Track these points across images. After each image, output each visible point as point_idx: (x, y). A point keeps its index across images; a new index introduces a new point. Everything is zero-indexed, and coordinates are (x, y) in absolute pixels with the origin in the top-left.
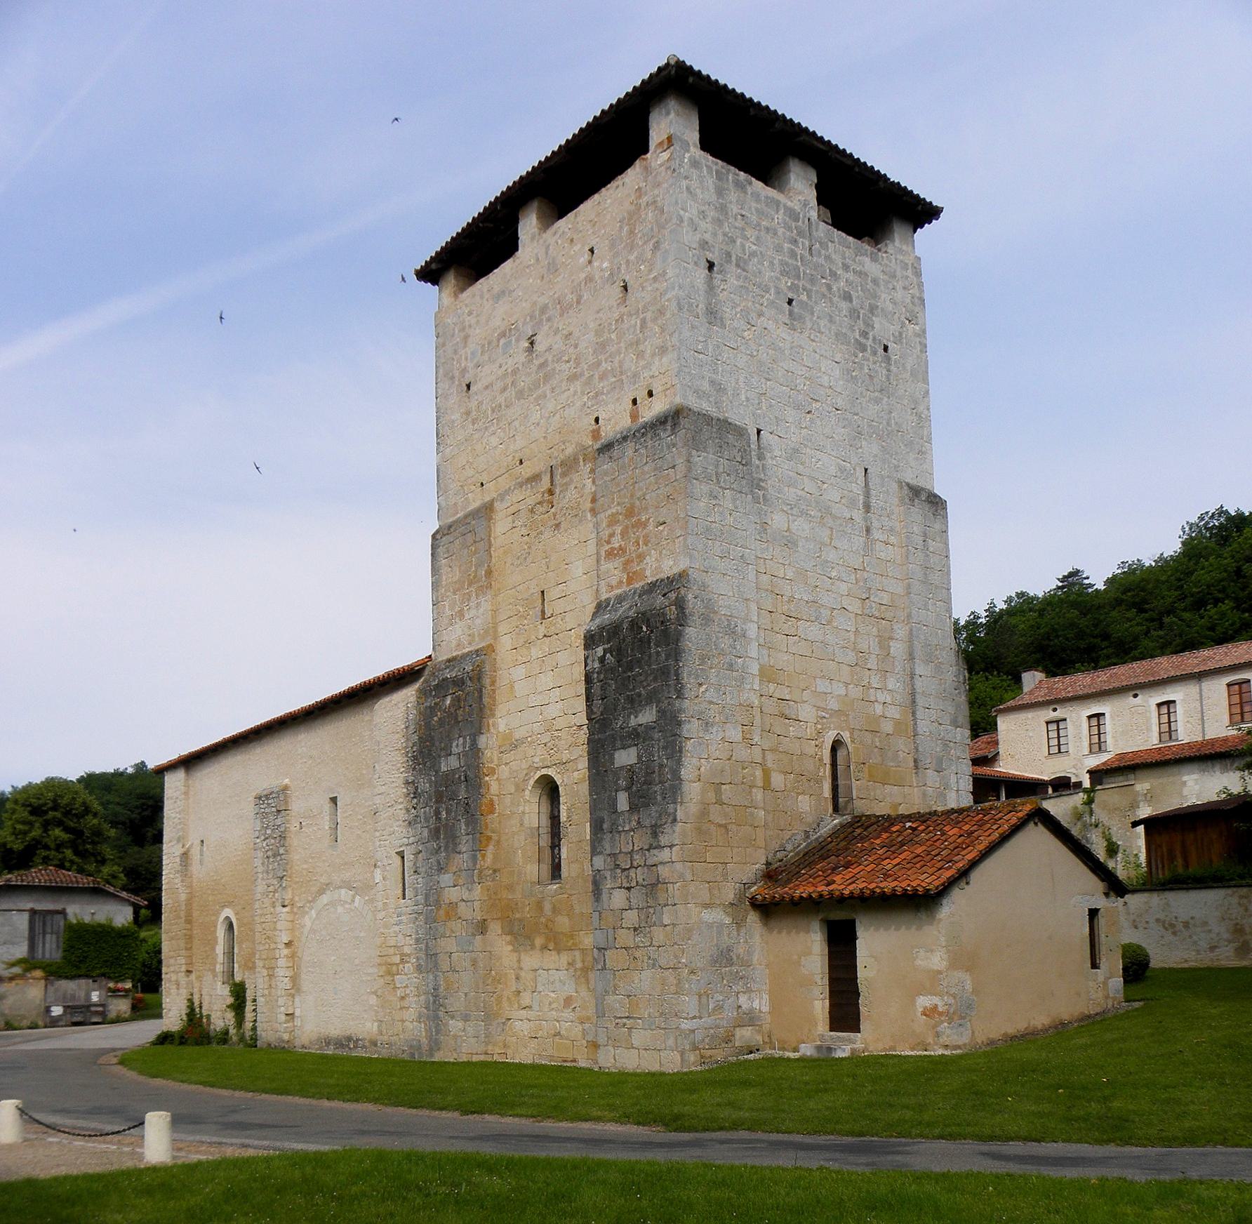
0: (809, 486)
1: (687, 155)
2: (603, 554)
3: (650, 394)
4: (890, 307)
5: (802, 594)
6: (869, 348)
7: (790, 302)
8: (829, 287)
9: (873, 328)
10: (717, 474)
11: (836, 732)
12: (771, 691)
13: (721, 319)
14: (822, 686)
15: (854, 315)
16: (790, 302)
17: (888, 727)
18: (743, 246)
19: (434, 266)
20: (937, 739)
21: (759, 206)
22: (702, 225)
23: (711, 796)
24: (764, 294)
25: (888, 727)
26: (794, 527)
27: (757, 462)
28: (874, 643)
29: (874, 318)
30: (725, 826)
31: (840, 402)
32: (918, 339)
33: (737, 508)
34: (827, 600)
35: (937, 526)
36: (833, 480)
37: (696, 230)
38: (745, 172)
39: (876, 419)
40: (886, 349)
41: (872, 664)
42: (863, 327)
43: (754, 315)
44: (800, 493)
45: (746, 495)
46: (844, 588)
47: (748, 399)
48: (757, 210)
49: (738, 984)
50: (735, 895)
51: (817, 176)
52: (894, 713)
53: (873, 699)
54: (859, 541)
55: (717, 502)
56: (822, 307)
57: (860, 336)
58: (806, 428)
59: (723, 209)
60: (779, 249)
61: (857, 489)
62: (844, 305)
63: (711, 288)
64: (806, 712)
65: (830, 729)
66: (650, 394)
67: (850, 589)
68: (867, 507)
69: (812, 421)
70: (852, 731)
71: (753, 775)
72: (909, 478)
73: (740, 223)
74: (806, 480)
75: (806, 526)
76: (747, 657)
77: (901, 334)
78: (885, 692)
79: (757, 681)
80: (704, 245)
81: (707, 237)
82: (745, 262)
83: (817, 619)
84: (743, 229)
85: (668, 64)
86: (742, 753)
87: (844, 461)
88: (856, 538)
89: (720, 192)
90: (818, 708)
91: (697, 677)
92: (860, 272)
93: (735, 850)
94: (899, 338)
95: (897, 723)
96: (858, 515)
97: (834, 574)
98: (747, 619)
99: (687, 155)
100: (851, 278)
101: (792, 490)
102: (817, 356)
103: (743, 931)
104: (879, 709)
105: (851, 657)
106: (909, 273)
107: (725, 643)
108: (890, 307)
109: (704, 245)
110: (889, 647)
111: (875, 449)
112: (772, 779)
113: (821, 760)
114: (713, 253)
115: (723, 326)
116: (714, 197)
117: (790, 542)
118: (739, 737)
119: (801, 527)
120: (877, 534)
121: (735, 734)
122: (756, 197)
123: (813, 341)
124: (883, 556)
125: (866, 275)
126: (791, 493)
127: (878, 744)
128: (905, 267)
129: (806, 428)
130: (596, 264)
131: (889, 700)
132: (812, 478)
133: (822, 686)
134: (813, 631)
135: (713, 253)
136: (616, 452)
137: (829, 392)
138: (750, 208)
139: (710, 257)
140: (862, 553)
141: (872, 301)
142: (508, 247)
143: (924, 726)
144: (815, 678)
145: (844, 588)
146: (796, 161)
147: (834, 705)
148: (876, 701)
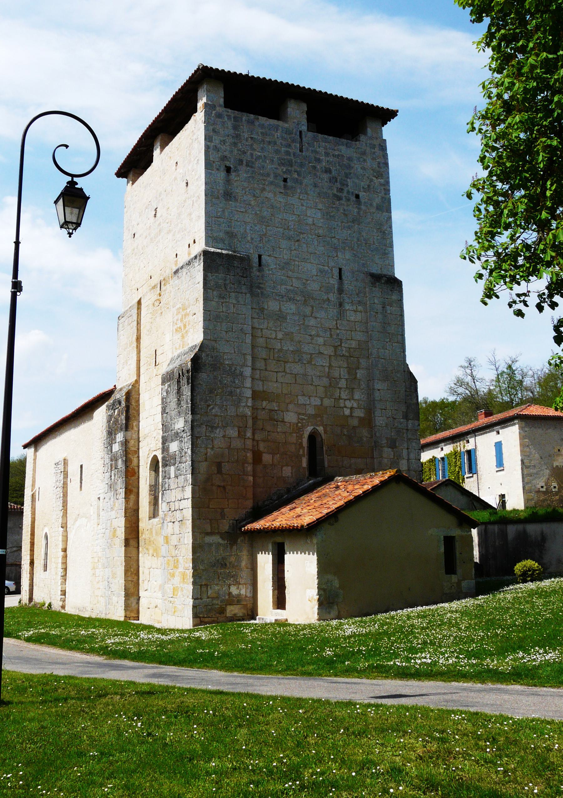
0: (296, 283)
1: (214, 112)
2: (174, 330)
3: (194, 242)
4: (360, 171)
5: (289, 347)
6: (344, 198)
7: (285, 180)
8: (314, 167)
9: (347, 185)
10: (225, 284)
11: (312, 427)
12: (264, 406)
13: (235, 197)
14: (302, 400)
15: (333, 180)
16: (285, 180)
17: (355, 422)
18: (252, 155)
19: (122, 171)
20: (391, 428)
21: (264, 131)
22: (224, 148)
23: (214, 469)
24: (265, 178)
25: (355, 422)
26: (283, 308)
27: (258, 273)
28: (344, 373)
29: (348, 180)
30: (224, 487)
31: (321, 232)
32: (382, 188)
33: (239, 302)
34: (306, 348)
35: (394, 297)
36: (315, 278)
37: (219, 151)
38: (254, 114)
39: (349, 239)
40: (357, 196)
41: (343, 384)
42: (339, 186)
43: (258, 191)
44: (289, 288)
45: (246, 294)
46: (321, 340)
47: (252, 239)
48: (262, 133)
49: (230, 580)
50: (230, 526)
51: (307, 107)
52: (360, 413)
53: (342, 405)
54: (333, 312)
55: (225, 300)
56: (308, 180)
57: (337, 191)
58: (295, 250)
59: (238, 136)
60: (277, 152)
61: (334, 281)
62: (326, 176)
63: (228, 181)
64: (291, 417)
65: (308, 426)
66: (194, 242)
67: (325, 341)
68: (341, 291)
69: (299, 246)
70: (325, 427)
71: (246, 456)
72: (375, 270)
73: (250, 142)
74: (294, 280)
75: (293, 307)
76: (244, 387)
77: (369, 186)
78: (352, 401)
79: (250, 400)
80: (224, 158)
81: (227, 154)
82: (253, 163)
83: (299, 360)
84: (252, 145)
85: (198, 69)
86: (237, 444)
87: (323, 266)
88: (331, 310)
89: (235, 128)
90: (299, 414)
91: (207, 401)
92: (339, 155)
93: (230, 501)
94: (368, 189)
95: (361, 419)
96: (333, 297)
97: (313, 333)
98: (244, 365)
99: (214, 112)
100: (331, 160)
101: (283, 287)
102: (304, 208)
103: (235, 547)
104: (347, 412)
105: (325, 381)
106: (377, 150)
107: (227, 380)
108: (360, 171)
109: (224, 158)
110: (356, 373)
111: (348, 255)
112: (263, 458)
113: (301, 444)
114: (230, 162)
115: (236, 200)
116: (232, 132)
117: (281, 317)
118: (236, 434)
119: (290, 308)
120: (347, 307)
121: (233, 432)
122: (262, 126)
123: (301, 199)
124: (352, 318)
125: (343, 156)
126: (282, 289)
127: (346, 433)
128: (373, 147)
129: (295, 250)
130: (178, 170)
131: (355, 405)
132: (298, 278)
133: (302, 400)
134: (297, 368)
135: (230, 162)
136: (180, 274)
137: (313, 227)
138: (257, 133)
139: (228, 164)
140: (336, 318)
141: (347, 171)
142: (149, 161)
143: (380, 420)
144: (297, 396)
145: (321, 340)
146: (292, 101)
147: (311, 411)
148: (345, 407)
